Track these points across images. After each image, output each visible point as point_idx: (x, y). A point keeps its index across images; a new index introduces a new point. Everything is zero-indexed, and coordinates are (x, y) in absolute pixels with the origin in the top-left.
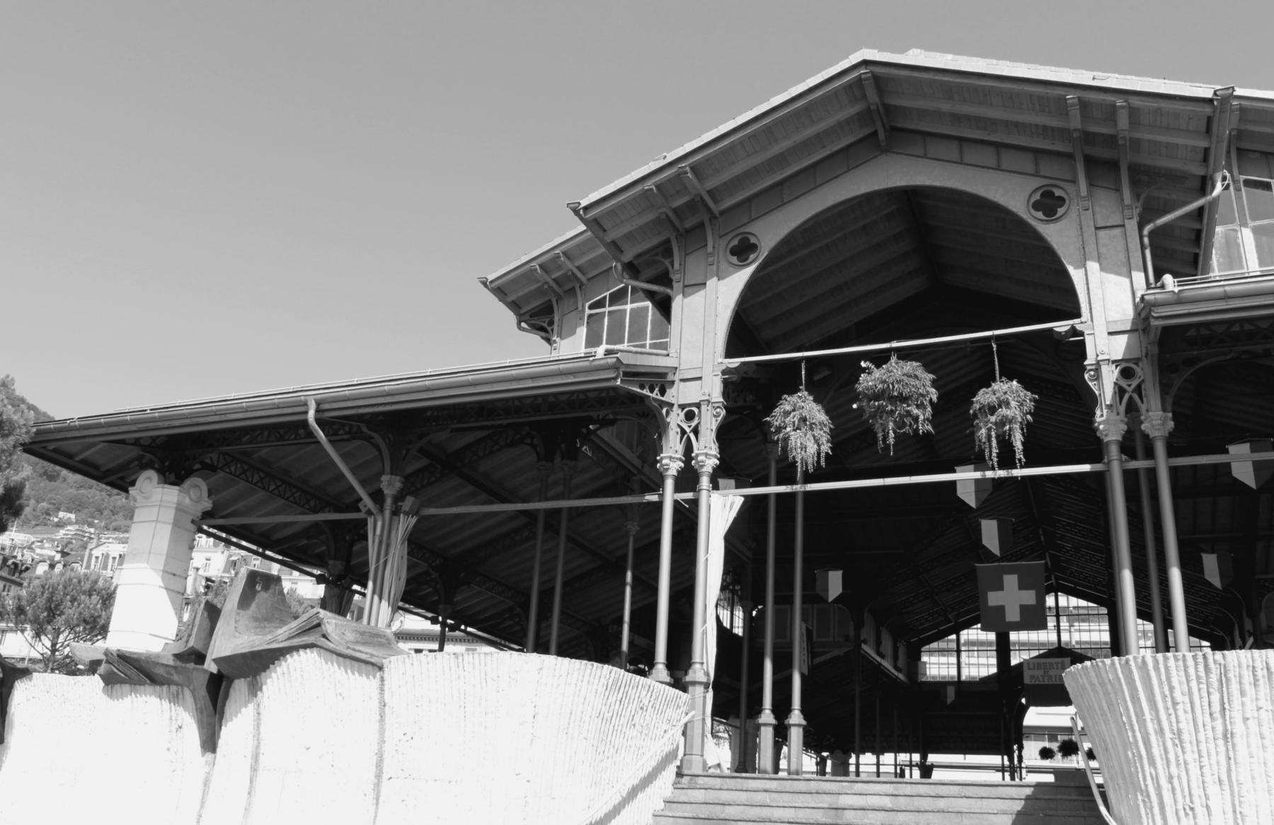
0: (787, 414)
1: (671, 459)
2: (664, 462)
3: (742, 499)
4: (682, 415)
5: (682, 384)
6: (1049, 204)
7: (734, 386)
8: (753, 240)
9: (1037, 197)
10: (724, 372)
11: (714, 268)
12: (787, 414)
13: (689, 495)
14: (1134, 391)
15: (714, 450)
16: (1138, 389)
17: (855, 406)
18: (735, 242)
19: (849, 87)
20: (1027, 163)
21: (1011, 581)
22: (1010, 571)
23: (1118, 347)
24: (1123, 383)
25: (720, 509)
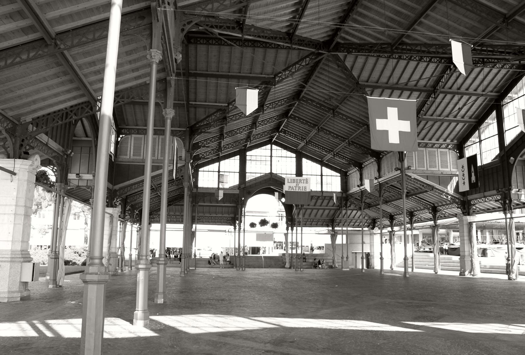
21: (392, 112)
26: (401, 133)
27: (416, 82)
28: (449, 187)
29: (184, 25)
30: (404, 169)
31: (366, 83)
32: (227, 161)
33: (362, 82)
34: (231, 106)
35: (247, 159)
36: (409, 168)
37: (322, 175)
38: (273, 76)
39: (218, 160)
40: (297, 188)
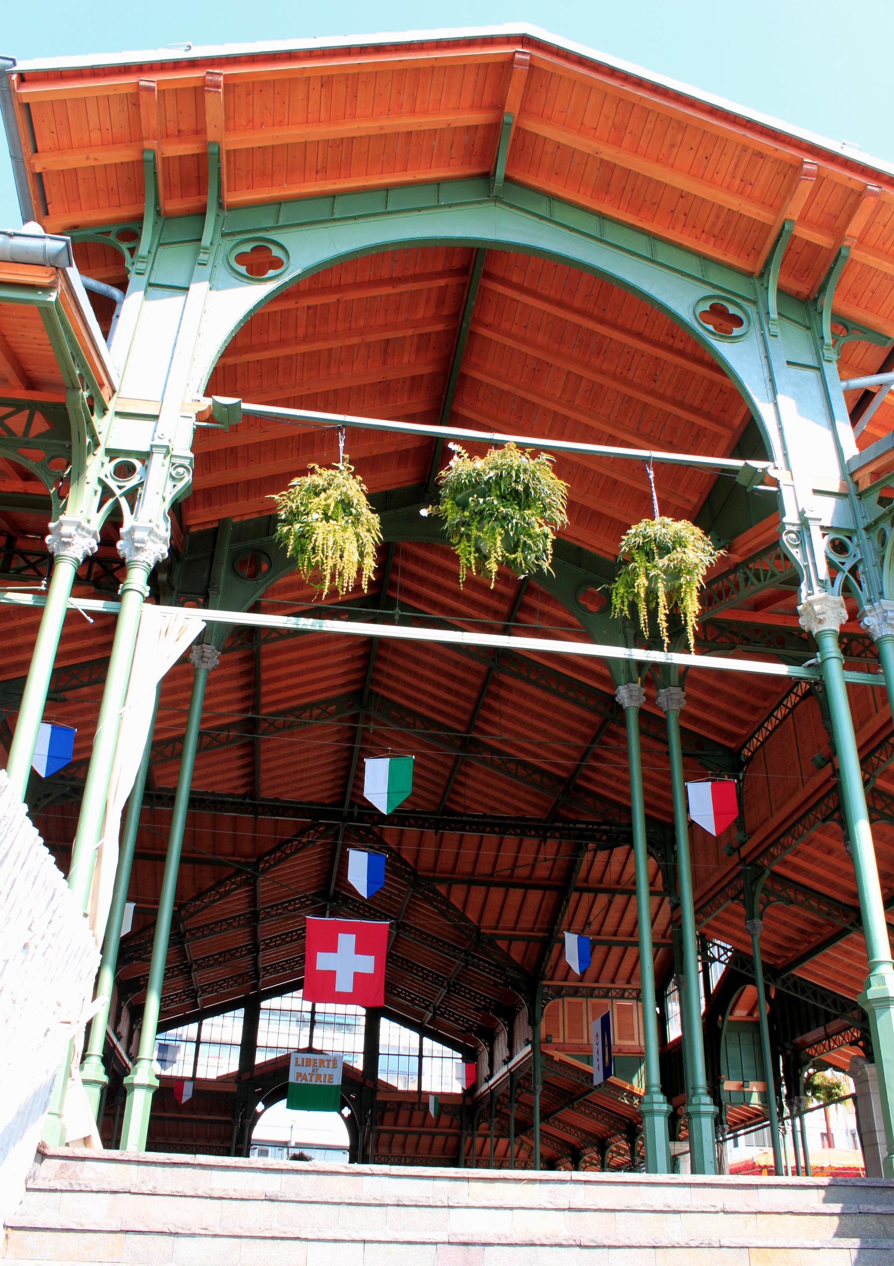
0: (316, 491)
1: (76, 529)
2: (65, 530)
3: (204, 624)
4: (110, 467)
5: (119, 421)
6: (724, 319)
7: (214, 445)
8: (276, 252)
9: (706, 306)
10: (200, 416)
11: (207, 270)
12: (316, 491)
13: (98, 605)
14: (850, 571)
15: (164, 530)
16: (853, 570)
17: (424, 512)
18: (247, 248)
19: (485, 67)
20: (692, 265)
21: (347, 941)
22: (348, 930)
23: (825, 511)
24: (836, 558)
25: (154, 639)
26: (357, 976)
27: (509, 871)
28: (635, 1081)
29: (39, 799)
30: (537, 1042)
31: (431, 875)
32: (217, 1020)
33: (425, 871)
34: (183, 912)
35: (364, 1019)
36: (548, 1040)
37: (421, 1056)
38: (255, 860)
39: (198, 1017)
40: (314, 1078)
